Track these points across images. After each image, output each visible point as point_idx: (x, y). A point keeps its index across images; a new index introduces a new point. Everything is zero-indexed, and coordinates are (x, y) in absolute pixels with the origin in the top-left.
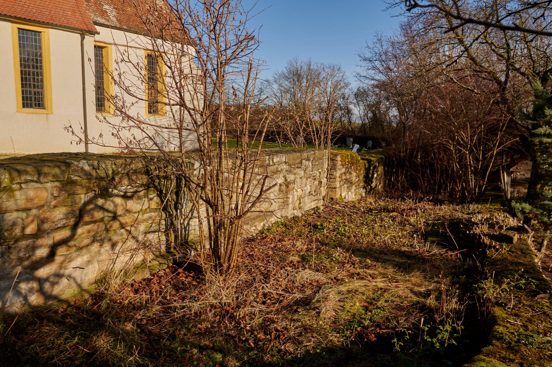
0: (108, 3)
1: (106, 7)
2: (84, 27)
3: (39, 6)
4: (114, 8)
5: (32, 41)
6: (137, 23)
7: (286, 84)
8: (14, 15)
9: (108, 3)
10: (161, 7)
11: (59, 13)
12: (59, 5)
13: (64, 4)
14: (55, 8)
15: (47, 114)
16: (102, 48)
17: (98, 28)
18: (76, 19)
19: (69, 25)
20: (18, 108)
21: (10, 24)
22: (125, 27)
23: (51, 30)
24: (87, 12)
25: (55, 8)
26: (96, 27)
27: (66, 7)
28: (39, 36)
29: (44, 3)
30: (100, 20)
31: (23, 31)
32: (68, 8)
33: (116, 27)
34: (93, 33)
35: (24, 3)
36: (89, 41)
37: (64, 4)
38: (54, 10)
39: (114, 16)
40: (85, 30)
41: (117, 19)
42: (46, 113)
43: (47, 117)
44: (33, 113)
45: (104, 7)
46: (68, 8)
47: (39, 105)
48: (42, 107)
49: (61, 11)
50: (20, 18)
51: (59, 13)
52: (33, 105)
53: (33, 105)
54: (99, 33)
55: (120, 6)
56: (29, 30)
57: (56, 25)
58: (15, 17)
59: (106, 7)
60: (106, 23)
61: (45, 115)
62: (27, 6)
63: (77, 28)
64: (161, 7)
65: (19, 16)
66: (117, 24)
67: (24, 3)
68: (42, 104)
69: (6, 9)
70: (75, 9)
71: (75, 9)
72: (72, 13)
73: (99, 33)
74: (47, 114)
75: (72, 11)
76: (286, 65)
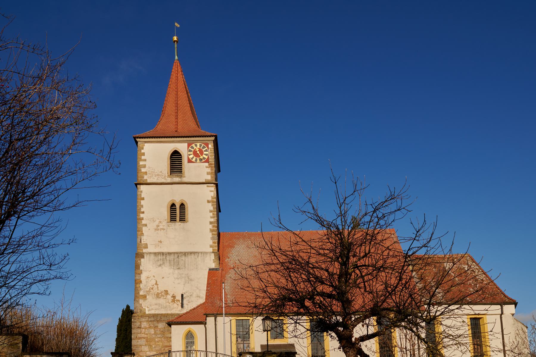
56: (243, 320)
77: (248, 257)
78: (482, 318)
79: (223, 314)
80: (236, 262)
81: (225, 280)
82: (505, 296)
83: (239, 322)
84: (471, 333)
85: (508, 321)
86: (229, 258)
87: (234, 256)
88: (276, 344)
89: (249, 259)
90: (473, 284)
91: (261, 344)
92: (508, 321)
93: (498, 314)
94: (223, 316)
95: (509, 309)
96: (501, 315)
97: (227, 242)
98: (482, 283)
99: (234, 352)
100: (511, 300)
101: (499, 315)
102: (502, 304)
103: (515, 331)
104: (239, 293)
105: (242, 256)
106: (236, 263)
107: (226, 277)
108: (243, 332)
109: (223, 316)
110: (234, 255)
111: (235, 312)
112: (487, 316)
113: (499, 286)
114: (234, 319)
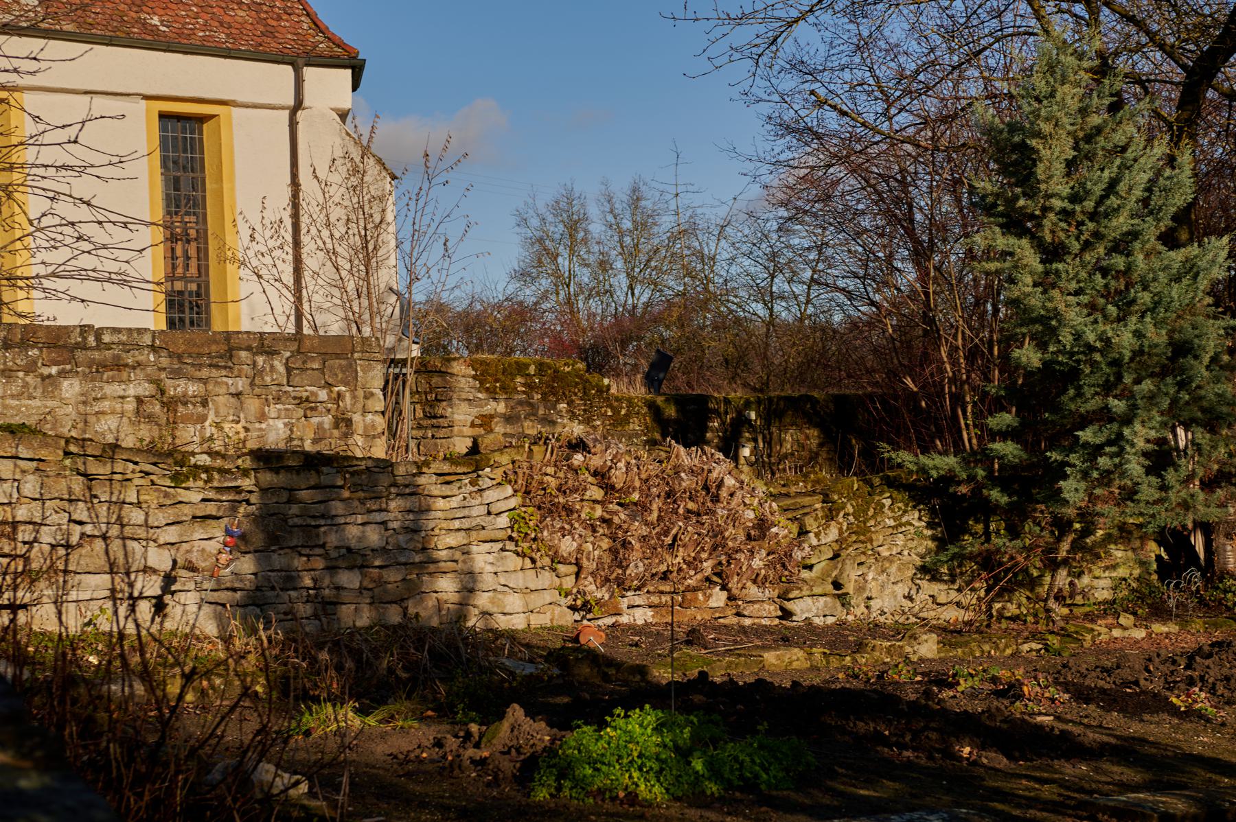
93: (283, 108)
100: (339, 46)
101: (287, 113)
102: (300, 61)
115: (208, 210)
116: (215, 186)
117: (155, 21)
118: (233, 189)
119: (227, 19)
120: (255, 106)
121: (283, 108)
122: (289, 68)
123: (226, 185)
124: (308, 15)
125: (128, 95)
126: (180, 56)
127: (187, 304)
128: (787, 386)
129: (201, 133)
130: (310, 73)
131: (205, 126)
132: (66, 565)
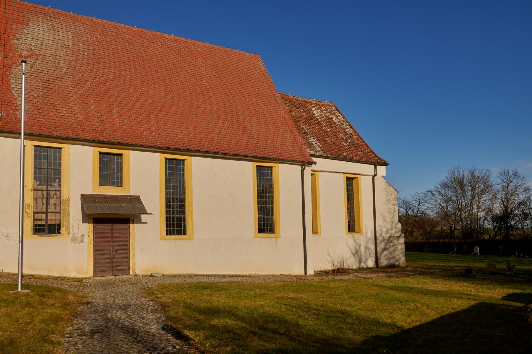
0: (312, 136)
1: (311, 140)
2: (303, 159)
3: (270, 146)
4: (317, 140)
5: (266, 176)
6: (337, 151)
7: (449, 193)
8: (255, 155)
9: (312, 136)
10: (351, 134)
11: (284, 150)
12: (283, 143)
13: (286, 142)
14: (281, 145)
15: (276, 238)
16: (353, 179)
17: (315, 159)
18: (297, 153)
19: (294, 159)
20: (255, 234)
21: (251, 163)
22: (329, 156)
23: (281, 165)
24: (303, 146)
25: (281, 145)
26: (312, 158)
27: (288, 144)
28: (271, 170)
29: (272, 143)
30: (309, 151)
31: (169, 160)
32: (289, 144)
33: (322, 156)
34: (311, 163)
35: (259, 145)
36: (308, 170)
37: (286, 142)
38: (280, 147)
39: (319, 147)
40: (305, 162)
41: (321, 149)
42: (275, 236)
43: (276, 240)
44: (266, 238)
45: (310, 140)
46: (289, 144)
47: (270, 231)
48: (272, 231)
49: (285, 148)
50: (259, 158)
51: (284, 150)
52: (266, 230)
53: (266, 230)
54: (315, 163)
55: (321, 138)
56: (48, 147)
57: (285, 160)
58: (257, 157)
59: (311, 140)
60: (315, 153)
61: (275, 238)
62: (262, 147)
63: (299, 161)
64: (351, 134)
65: (259, 156)
66: (323, 153)
67: (259, 145)
68: (272, 228)
69: (249, 151)
70: (294, 144)
71: (294, 144)
72: (293, 148)
73: (315, 163)
74: (276, 238)
75: (292, 147)
76: (447, 175)
77: (54, 46)
78: (356, 178)
79: (20, 134)
80: (33, 48)
81: (11, 73)
82: (379, 158)
83: (41, 151)
84: (4, 271)
85: (380, 183)
86: (17, 39)
87: (29, 39)
88: (108, 195)
89: (56, 48)
90: (344, 138)
91: (83, 193)
92: (380, 183)
93: (369, 176)
94: (20, 138)
95: (382, 170)
96: (374, 177)
97: (13, 13)
98: (352, 138)
99: (29, 205)
100: (382, 160)
101: (372, 177)
102: (376, 164)
103: (386, 196)
104: (40, 101)
105: (43, 42)
106: (31, 50)
107: (12, 68)
108: (48, 169)
109: (20, 138)
110: (26, 36)
111: (34, 132)
112: (362, 177)
113: (367, 143)
114: (30, 144)
115: (354, 202)
116: (357, 195)
117: (344, 154)
118: (361, 196)
119: (358, 154)
120: (366, 175)
121: (369, 176)
122: (373, 166)
123: (360, 195)
124: (373, 153)
125: (341, 173)
126: (351, 163)
127: (175, 211)
128: (380, 228)
129: (353, 182)
130: (378, 167)
131: (354, 180)
132: (47, 209)
